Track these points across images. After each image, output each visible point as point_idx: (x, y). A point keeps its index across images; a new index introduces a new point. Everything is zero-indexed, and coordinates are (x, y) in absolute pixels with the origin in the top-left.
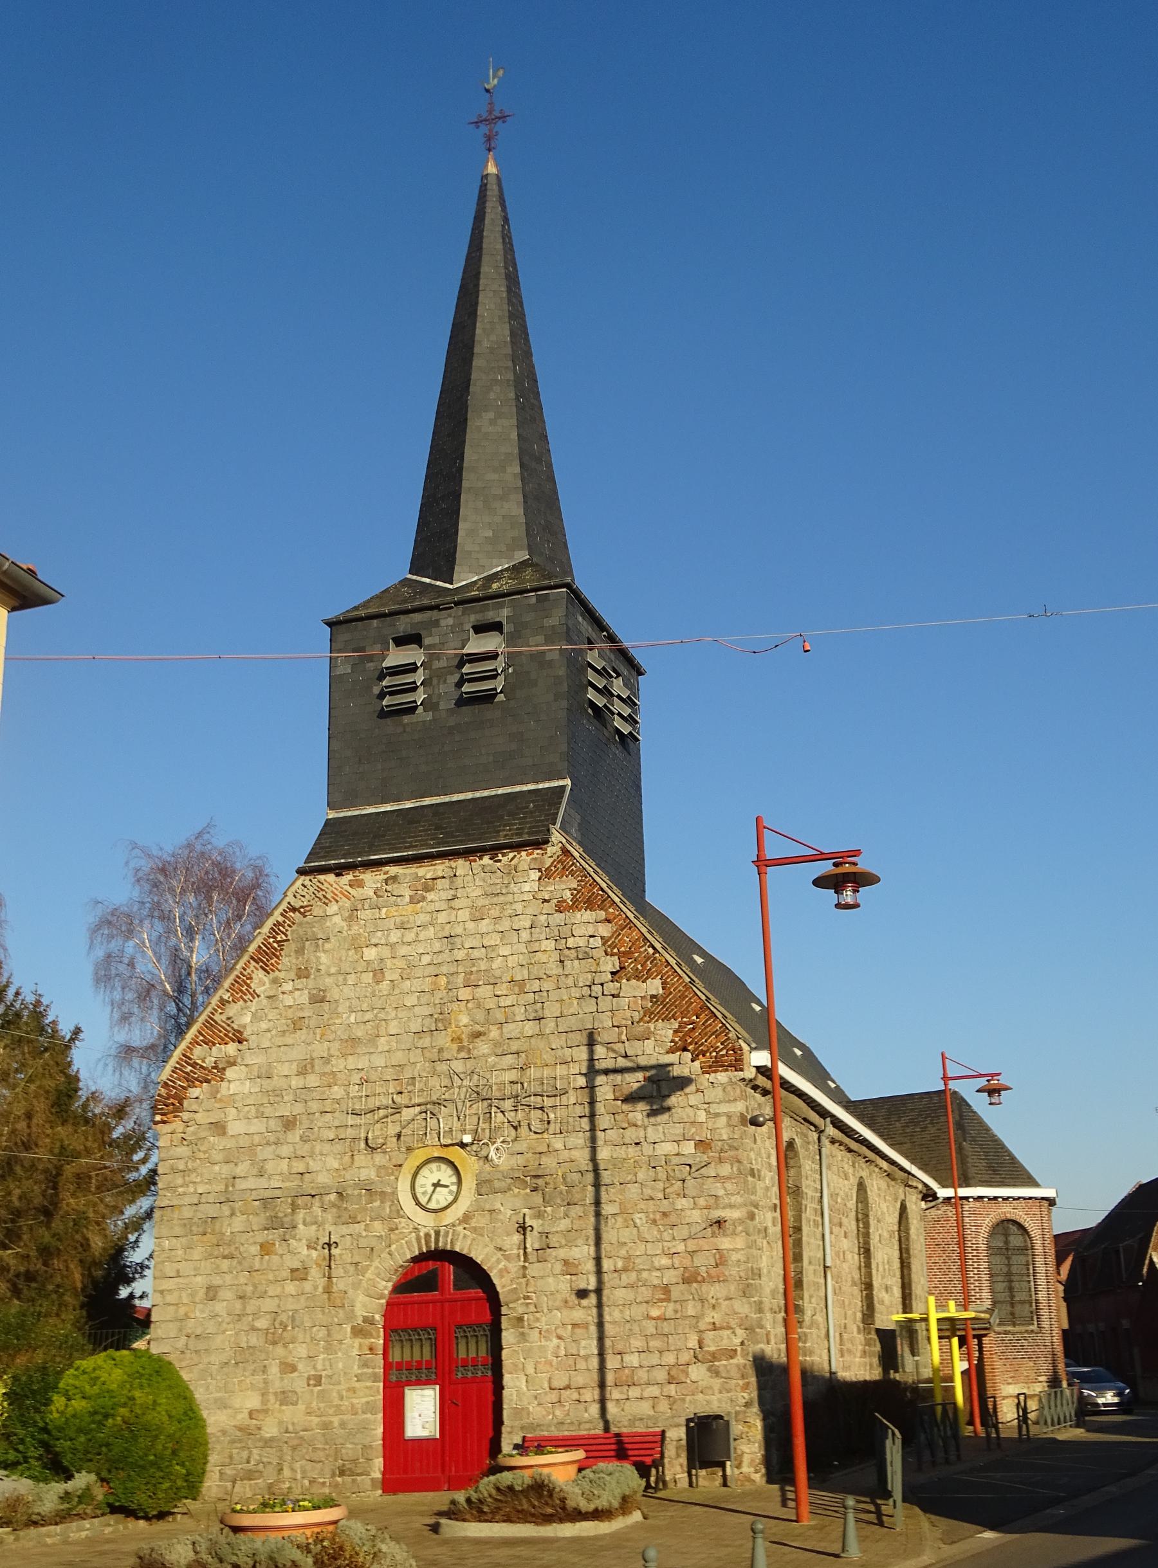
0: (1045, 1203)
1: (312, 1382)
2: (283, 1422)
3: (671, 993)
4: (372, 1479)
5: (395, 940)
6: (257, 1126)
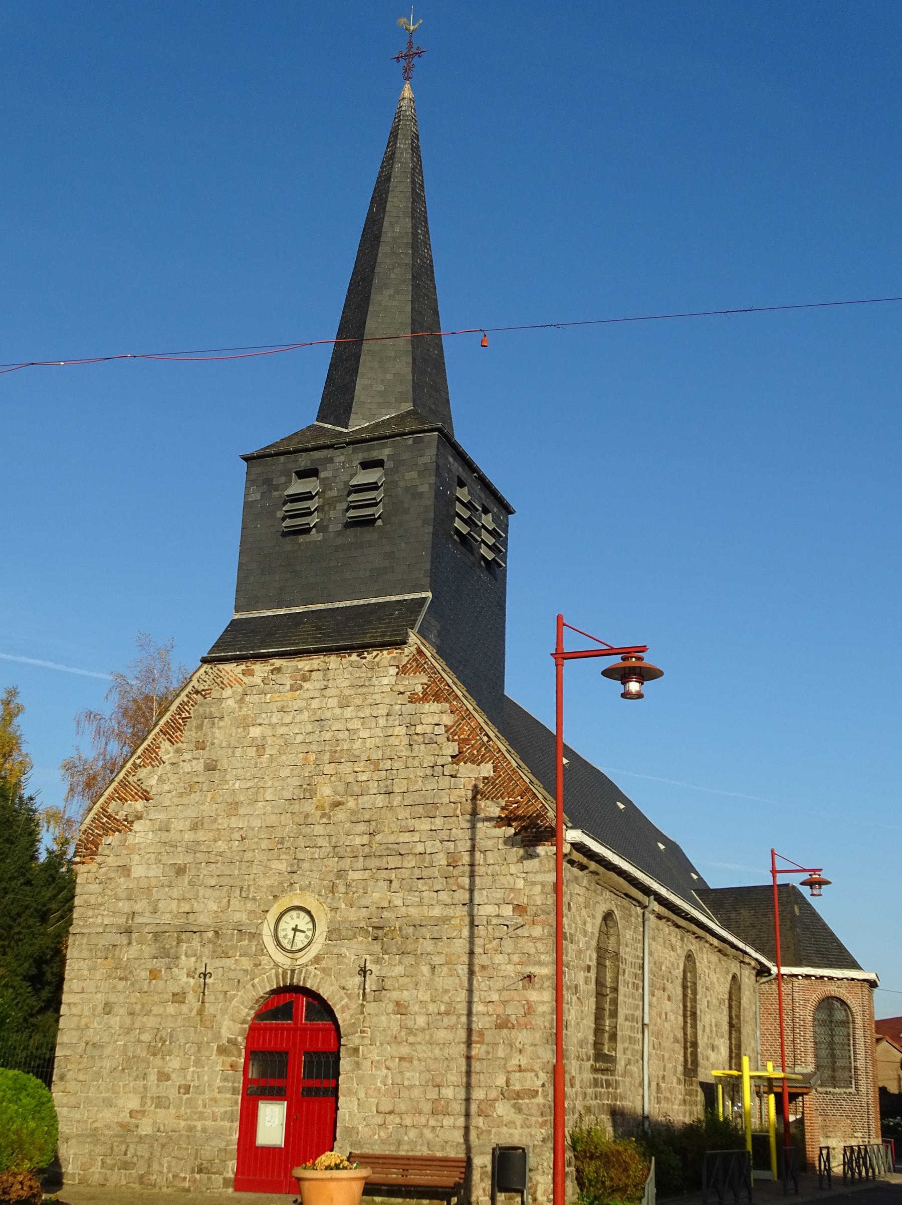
0: (866, 985)
1: (182, 1090)
2: (156, 1123)
3: (500, 776)
4: (224, 1179)
5: (276, 721)
6: (155, 871)
